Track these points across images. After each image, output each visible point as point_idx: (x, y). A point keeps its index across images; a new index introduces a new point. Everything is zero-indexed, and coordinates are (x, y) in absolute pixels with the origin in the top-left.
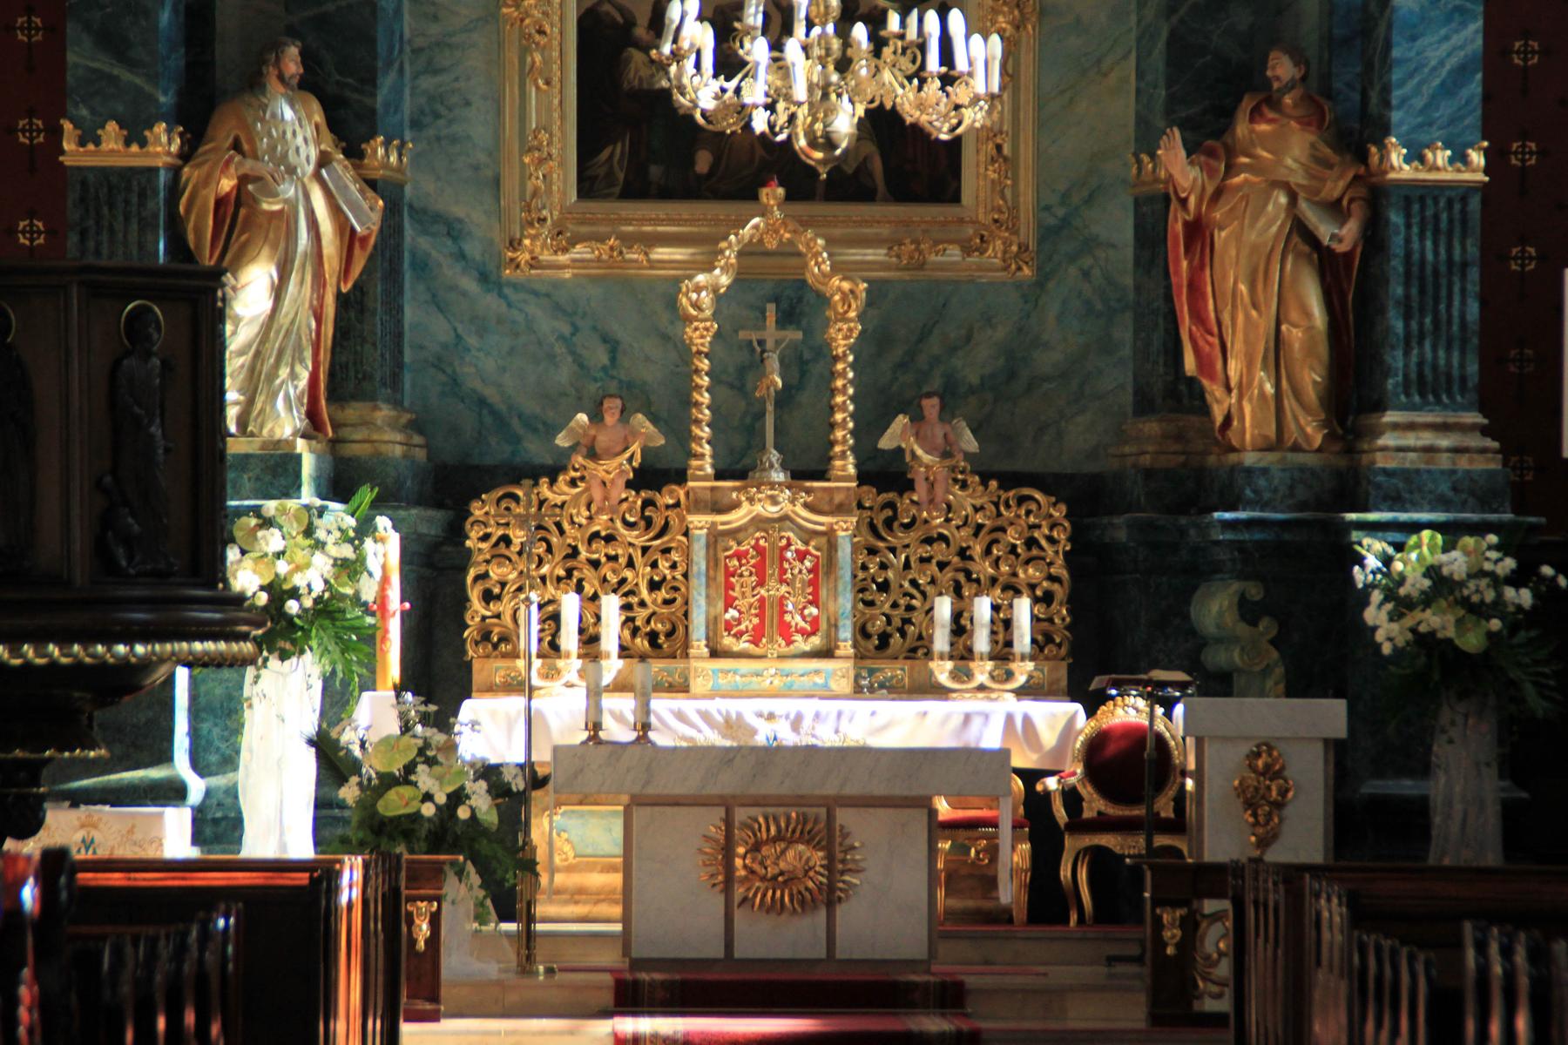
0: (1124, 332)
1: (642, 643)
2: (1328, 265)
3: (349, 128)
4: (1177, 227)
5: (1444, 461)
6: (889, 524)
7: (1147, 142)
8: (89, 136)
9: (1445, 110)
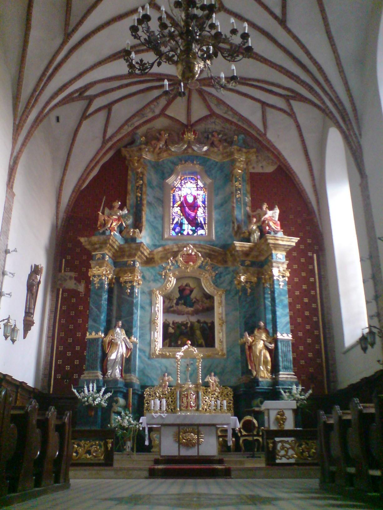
0: (240, 366)
1: (170, 410)
2: (270, 351)
3: (129, 333)
4: (247, 347)
5: (289, 380)
6: (206, 392)
7: (242, 336)
8: (91, 334)
9: (285, 329)
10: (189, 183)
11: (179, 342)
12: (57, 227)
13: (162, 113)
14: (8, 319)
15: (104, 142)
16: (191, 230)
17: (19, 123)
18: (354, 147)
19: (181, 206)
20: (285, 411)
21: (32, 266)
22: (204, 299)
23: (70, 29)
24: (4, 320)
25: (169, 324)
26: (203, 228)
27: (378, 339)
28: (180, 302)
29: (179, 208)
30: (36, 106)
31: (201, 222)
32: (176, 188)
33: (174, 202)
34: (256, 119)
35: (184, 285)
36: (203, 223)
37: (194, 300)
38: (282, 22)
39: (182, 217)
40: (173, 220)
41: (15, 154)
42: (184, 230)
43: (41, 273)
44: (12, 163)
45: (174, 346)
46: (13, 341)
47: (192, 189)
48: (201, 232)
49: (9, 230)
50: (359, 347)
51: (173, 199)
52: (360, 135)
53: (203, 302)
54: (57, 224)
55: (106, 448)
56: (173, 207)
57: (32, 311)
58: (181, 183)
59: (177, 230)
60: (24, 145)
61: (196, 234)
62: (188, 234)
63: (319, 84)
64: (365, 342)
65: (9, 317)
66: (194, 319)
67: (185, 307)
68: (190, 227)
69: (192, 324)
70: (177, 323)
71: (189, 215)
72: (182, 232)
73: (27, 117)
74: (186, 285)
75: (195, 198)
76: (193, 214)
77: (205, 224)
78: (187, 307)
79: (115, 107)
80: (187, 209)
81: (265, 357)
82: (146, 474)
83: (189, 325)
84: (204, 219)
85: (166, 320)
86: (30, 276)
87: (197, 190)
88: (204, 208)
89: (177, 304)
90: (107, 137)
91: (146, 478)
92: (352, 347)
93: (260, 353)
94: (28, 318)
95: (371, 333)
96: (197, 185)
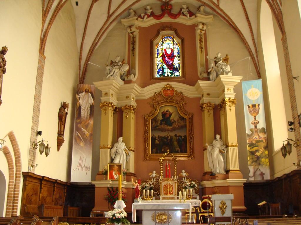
10: (168, 40)
11: (163, 150)
12: (79, 75)
14: (42, 141)
15: (109, 16)
16: (170, 72)
17: (47, 9)
18: (277, 13)
19: (163, 57)
21: (61, 103)
22: (179, 120)
24: (40, 141)
25: (156, 138)
26: (178, 71)
27: (294, 149)
28: (163, 123)
29: (161, 58)
31: (177, 67)
32: (159, 44)
35: (166, 111)
36: (178, 67)
37: (172, 121)
39: (163, 64)
40: (157, 66)
41: (44, 30)
42: (165, 73)
43: (68, 107)
44: (42, 37)
45: (159, 153)
46: (47, 154)
47: (170, 45)
48: (177, 74)
49: (42, 81)
50: (281, 154)
51: (157, 52)
52: (281, 4)
53: (178, 122)
54: (79, 73)
56: (157, 57)
57: (62, 133)
58: (162, 41)
59: (160, 73)
60: (50, 23)
61: (173, 76)
62: (168, 75)
64: (286, 150)
65: (43, 140)
66: (172, 134)
67: (166, 126)
68: (169, 70)
69: (171, 137)
70: (161, 137)
72: (164, 74)
73: (52, 5)
74: (167, 111)
75: (172, 51)
76: (171, 62)
77: (179, 68)
80: (167, 59)
81: (220, 161)
83: (169, 138)
86: (60, 110)
87: (174, 45)
88: (179, 57)
89: (161, 124)
90: (110, 13)
92: (278, 152)
94: (61, 138)
95: (289, 144)
96: (173, 42)
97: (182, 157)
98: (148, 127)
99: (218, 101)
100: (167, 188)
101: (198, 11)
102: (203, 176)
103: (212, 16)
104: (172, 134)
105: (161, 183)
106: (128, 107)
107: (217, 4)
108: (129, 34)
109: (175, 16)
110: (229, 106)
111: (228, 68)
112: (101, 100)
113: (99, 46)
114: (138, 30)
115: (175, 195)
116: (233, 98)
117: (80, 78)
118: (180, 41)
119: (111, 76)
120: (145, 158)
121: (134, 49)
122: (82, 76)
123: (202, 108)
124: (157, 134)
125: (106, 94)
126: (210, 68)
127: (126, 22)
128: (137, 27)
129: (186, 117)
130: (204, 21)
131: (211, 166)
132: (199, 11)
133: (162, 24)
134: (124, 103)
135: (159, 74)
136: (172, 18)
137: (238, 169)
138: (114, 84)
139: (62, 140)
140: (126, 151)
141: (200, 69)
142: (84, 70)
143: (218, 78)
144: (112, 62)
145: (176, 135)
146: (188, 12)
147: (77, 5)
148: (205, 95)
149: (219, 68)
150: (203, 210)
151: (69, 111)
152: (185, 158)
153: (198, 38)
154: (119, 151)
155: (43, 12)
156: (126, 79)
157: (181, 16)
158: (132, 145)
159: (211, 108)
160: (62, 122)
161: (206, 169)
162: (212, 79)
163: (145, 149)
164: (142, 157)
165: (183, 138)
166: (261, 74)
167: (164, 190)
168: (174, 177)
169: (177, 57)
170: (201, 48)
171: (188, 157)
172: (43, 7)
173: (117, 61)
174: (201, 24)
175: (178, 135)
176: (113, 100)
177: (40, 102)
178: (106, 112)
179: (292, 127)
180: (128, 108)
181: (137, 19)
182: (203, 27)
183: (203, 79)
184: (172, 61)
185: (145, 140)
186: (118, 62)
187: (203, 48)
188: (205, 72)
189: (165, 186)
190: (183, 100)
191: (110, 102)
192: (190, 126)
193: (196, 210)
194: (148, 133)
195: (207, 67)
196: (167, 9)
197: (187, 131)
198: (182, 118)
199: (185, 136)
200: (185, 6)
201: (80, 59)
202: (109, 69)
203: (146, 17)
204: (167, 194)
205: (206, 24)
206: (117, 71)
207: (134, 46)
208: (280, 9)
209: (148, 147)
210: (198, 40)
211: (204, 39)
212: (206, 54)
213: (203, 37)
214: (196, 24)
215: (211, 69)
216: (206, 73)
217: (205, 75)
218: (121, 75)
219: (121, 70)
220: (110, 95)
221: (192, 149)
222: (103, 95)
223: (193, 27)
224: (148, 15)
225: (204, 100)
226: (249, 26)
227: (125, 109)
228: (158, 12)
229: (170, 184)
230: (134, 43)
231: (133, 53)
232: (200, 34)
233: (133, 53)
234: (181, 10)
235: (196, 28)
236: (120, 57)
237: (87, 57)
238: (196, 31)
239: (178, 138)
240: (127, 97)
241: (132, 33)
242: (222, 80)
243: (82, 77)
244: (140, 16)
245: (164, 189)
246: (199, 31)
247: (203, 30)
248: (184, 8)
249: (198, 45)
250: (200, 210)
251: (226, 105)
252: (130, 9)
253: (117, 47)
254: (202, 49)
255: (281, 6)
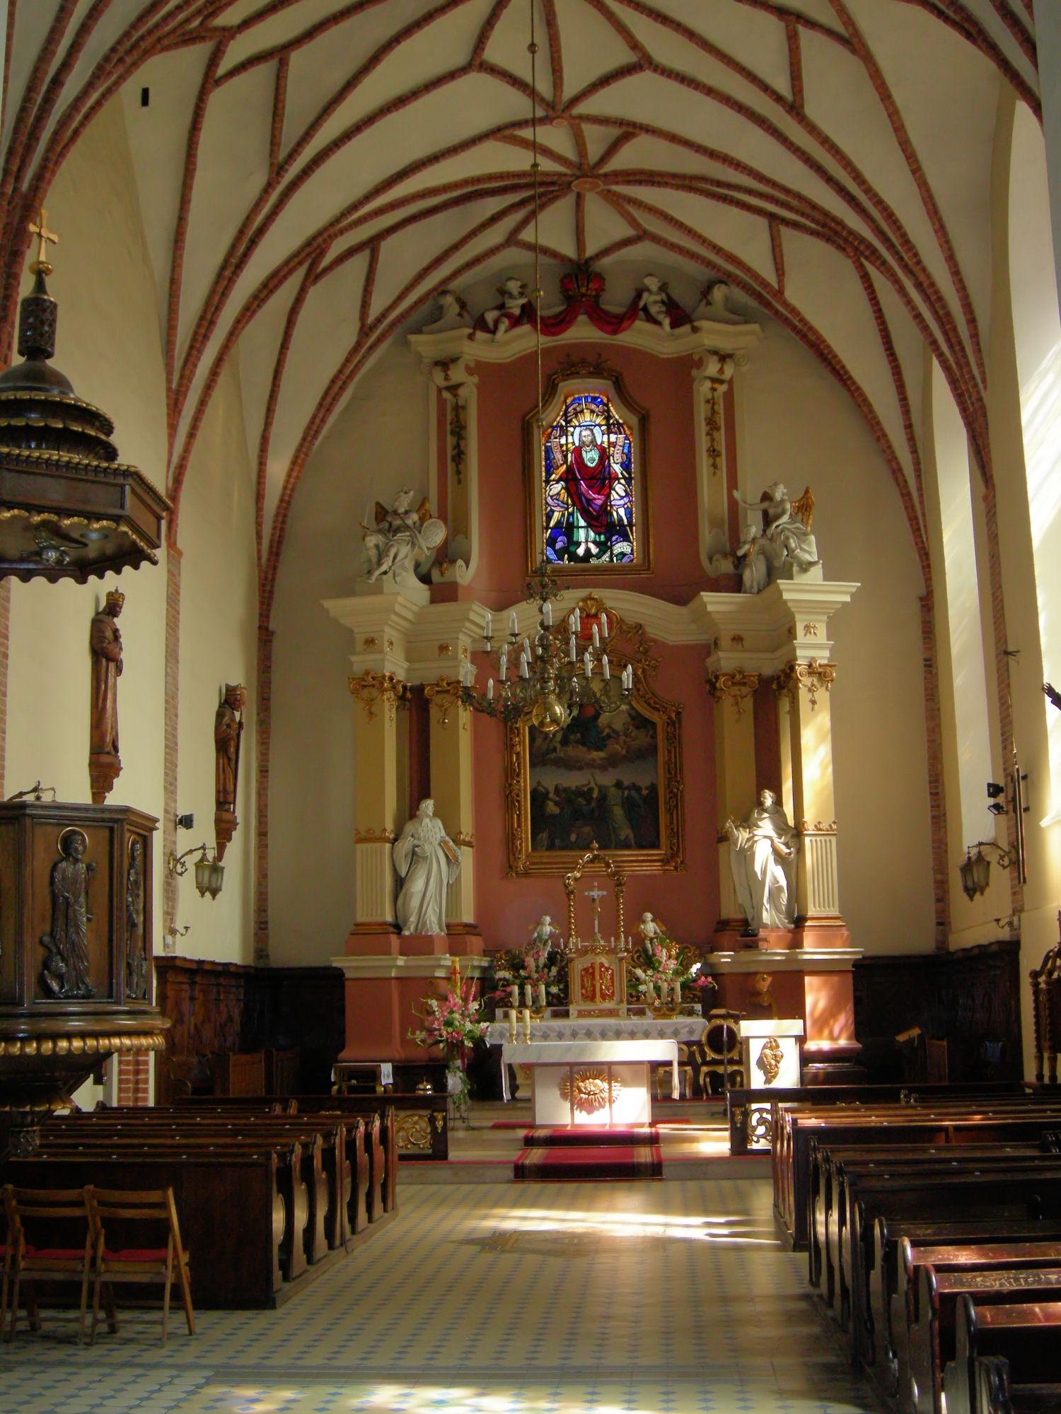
10: (587, 413)
11: (573, 837)
12: (259, 558)
13: (512, 239)
15: (365, 331)
16: (594, 542)
19: (569, 479)
20: (779, 1041)
23: (282, 155)
25: (548, 793)
30: (213, 337)
31: (620, 519)
32: (554, 428)
33: (550, 469)
34: (757, 255)
37: (607, 731)
38: (795, 109)
40: (549, 517)
41: (175, 460)
42: (579, 544)
44: (170, 484)
47: (597, 430)
48: (621, 547)
51: (547, 458)
52: (984, 381)
55: (434, 1128)
56: (547, 482)
58: (566, 412)
63: (891, 246)
66: (606, 779)
67: (584, 749)
70: (565, 790)
71: (590, 501)
72: (572, 549)
75: (604, 455)
77: (631, 525)
78: (589, 749)
79: (385, 246)
82: (511, 1174)
83: (595, 795)
84: (629, 513)
85: (539, 783)
86: (220, 715)
88: (628, 481)
89: (565, 742)
90: (371, 319)
91: (509, 1181)
93: (764, 873)
96: (608, 418)
97: (641, 864)
98: (518, 754)
99: (768, 666)
100: (593, 979)
101: (704, 302)
102: (716, 931)
103: (755, 327)
104: (606, 779)
105: (571, 960)
106: (448, 684)
107: (776, 286)
108: (440, 391)
109: (613, 323)
110: (810, 690)
111: (809, 550)
112: (351, 664)
113: (327, 438)
114: (475, 379)
115: (622, 1001)
116: (825, 662)
117: (260, 571)
118: (634, 420)
119: (385, 573)
120: (510, 867)
121: (459, 456)
122: (269, 560)
123: (711, 687)
124: (553, 779)
125: (370, 642)
126: (745, 543)
127: (426, 345)
128: (472, 364)
129: (655, 717)
130: (725, 345)
131: (742, 897)
132: (709, 303)
133: (568, 350)
134: (429, 672)
135: (553, 548)
136: (602, 330)
137: (835, 912)
138: (398, 608)
139: (229, 822)
140: (449, 848)
141: (707, 537)
142: (276, 538)
143: (772, 587)
144: (382, 513)
145: (619, 785)
146: (664, 309)
147: (145, 101)
148: (725, 642)
149: (777, 545)
150: (711, 1055)
151: (246, 714)
152: (654, 869)
153: (701, 412)
154: (424, 852)
155: (168, 397)
156: (436, 578)
157: (640, 324)
158: (467, 826)
159: (745, 690)
160: (229, 759)
161: (728, 911)
162: (752, 587)
163: (510, 839)
164: (501, 863)
165: (645, 792)
166: (931, 557)
167: (583, 986)
168: (617, 939)
169: (622, 481)
170: (713, 453)
171: (665, 861)
172: (169, 381)
173: (401, 510)
174: (715, 358)
175: (626, 783)
176: (395, 665)
177: (176, 716)
178: (373, 709)
179: (1001, 799)
180: (448, 691)
181: (471, 337)
182: (721, 371)
183: (716, 585)
184: (602, 497)
185: (510, 801)
186: (406, 512)
187: (719, 455)
188: (725, 556)
189: (586, 970)
190: (646, 652)
191: (387, 674)
192: (669, 751)
193: (692, 1054)
194: (518, 775)
195: (735, 539)
196: (583, 295)
197: (661, 771)
198: (640, 722)
199: (653, 788)
200: (653, 283)
201: (260, 497)
202: (377, 546)
203: (505, 323)
204: (593, 998)
205: (730, 356)
206: (405, 550)
207: (462, 443)
208: (980, 399)
209: (519, 826)
210: (703, 423)
211: (725, 419)
212: (733, 483)
213: (720, 408)
214: (696, 357)
215: (747, 547)
216: (730, 559)
217: (726, 566)
218: (417, 566)
219: (420, 547)
220: (386, 644)
221: (675, 834)
222: (359, 645)
223: (686, 366)
224: (509, 316)
225: (723, 663)
226: (894, 374)
227: (438, 692)
228: (548, 300)
229: (602, 965)
230: (459, 430)
231: (458, 472)
232: (709, 396)
233: (458, 472)
234: (639, 296)
235: (694, 372)
236: (412, 493)
237: (285, 488)
238: (695, 385)
239: (626, 793)
240: (443, 648)
241: (453, 389)
242: (786, 596)
243: (268, 566)
244: (480, 324)
245: (582, 981)
246: (708, 384)
247: (721, 382)
248: (648, 290)
249: (703, 443)
250: (703, 1054)
251: (797, 688)
252: (445, 293)
253: (393, 443)
254: (718, 459)
255: (985, 388)
